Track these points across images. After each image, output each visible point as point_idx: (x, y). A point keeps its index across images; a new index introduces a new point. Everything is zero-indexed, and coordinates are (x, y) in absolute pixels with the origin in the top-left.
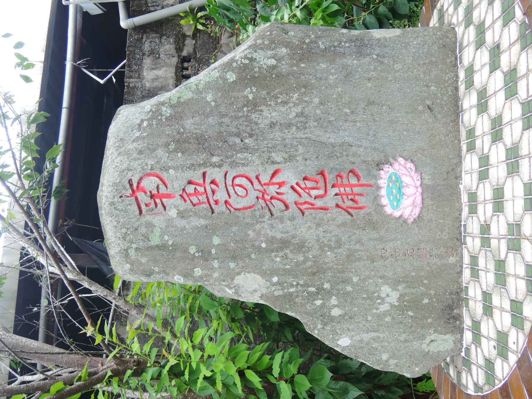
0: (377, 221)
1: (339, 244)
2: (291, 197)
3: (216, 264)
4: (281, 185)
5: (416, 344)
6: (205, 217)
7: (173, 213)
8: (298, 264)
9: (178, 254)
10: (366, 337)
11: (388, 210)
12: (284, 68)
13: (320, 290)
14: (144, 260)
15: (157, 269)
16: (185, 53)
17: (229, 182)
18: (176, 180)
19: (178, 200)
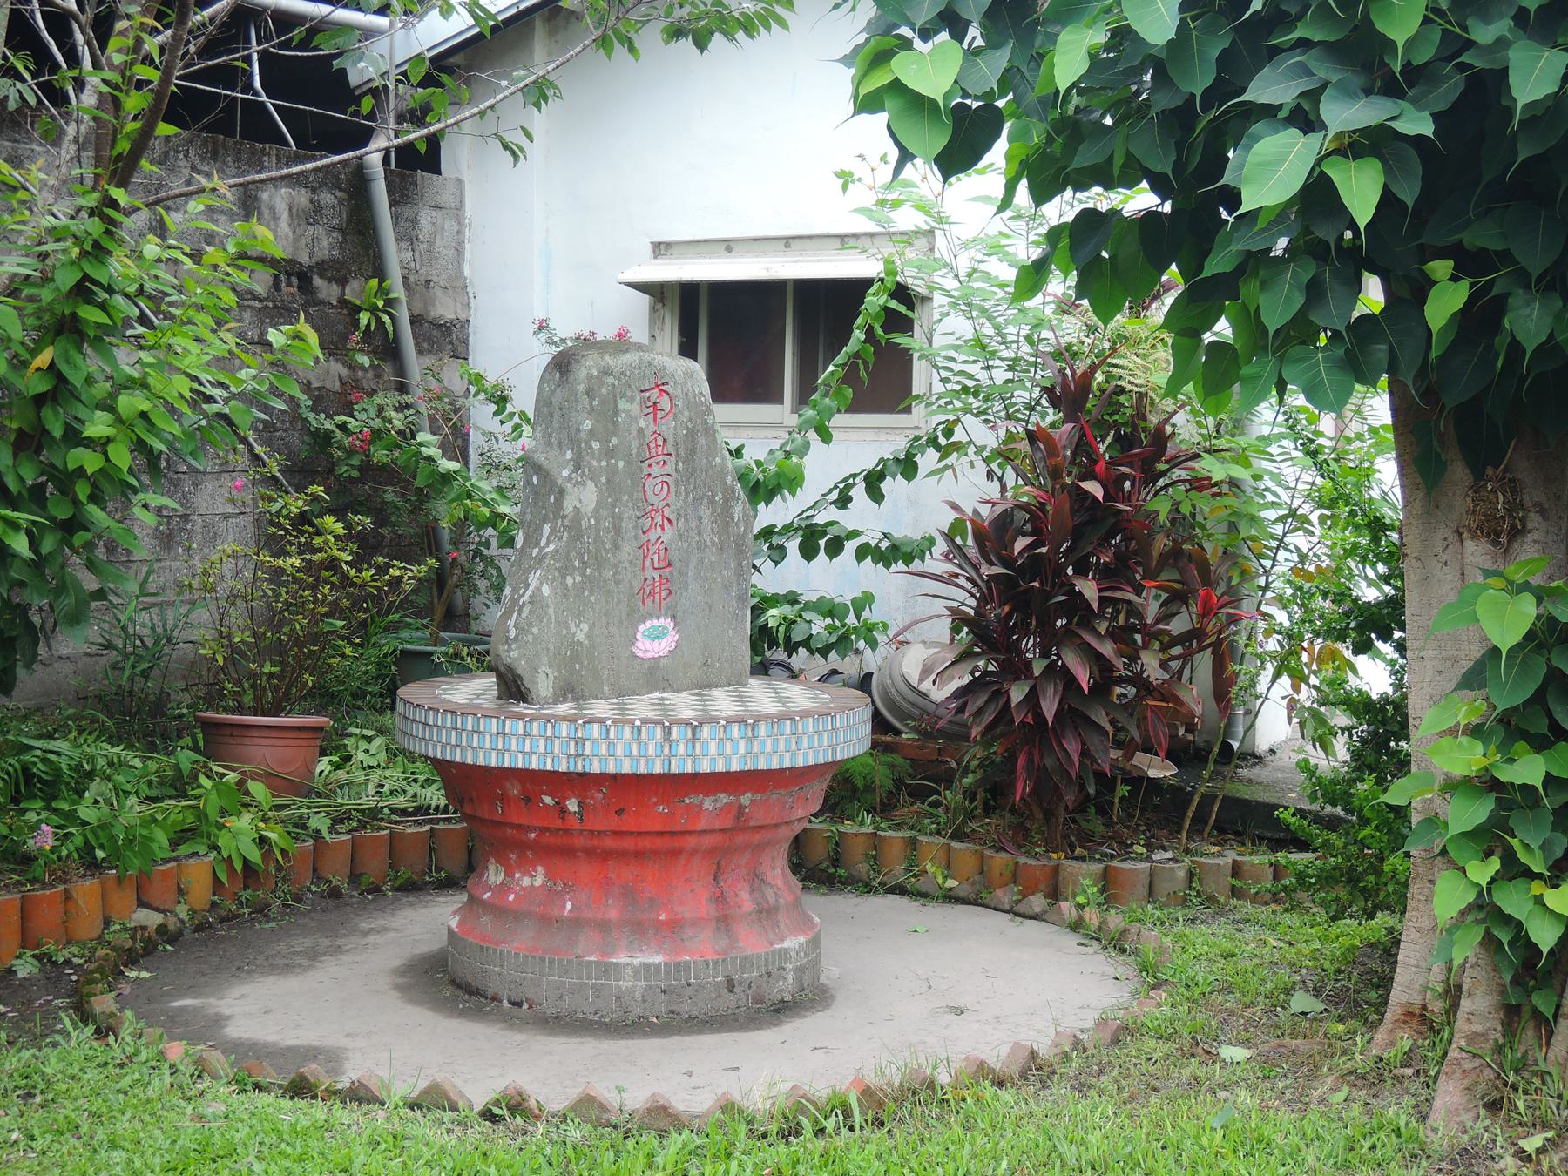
0: (635, 617)
1: (618, 582)
2: (652, 536)
3: (604, 463)
4: (663, 528)
5: (545, 660)
6: (638, 454)
7: (642, 423)
8: (603, 543)
9: (610, 426)
10: (551, 611)
11: (642, 628)
12: (733, 529)
13: (585, 564)
14: (604, 391)
15: (595, 403)
16: (317, 281)
17: (666, 478)
18: (668, 427)
19: (652, 428)
